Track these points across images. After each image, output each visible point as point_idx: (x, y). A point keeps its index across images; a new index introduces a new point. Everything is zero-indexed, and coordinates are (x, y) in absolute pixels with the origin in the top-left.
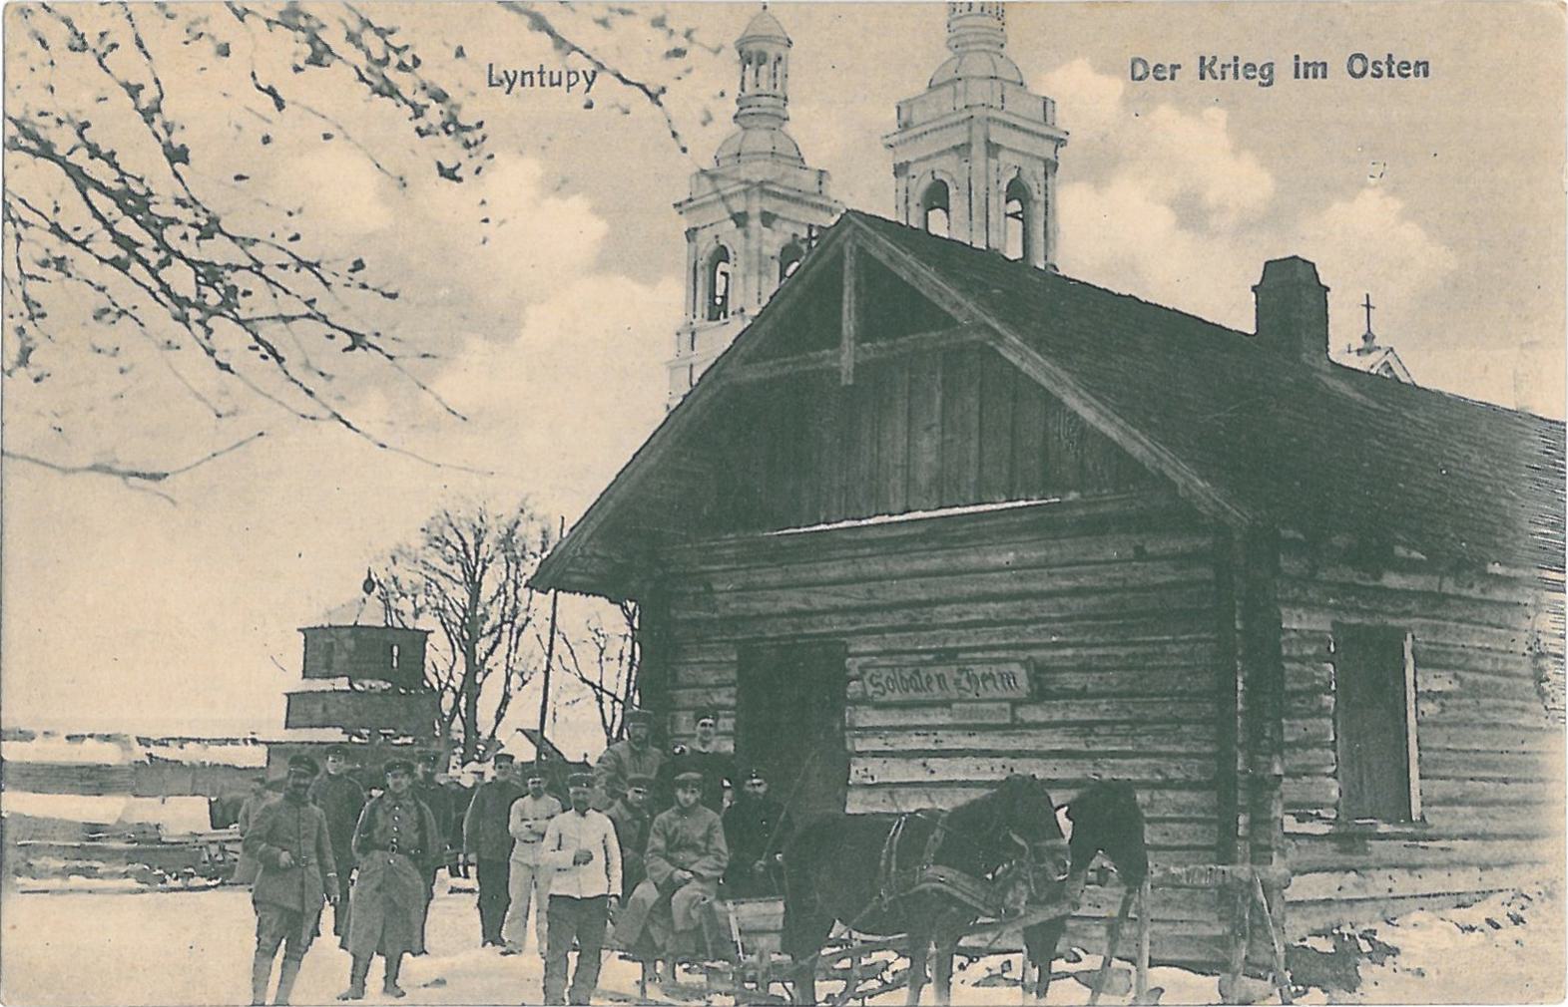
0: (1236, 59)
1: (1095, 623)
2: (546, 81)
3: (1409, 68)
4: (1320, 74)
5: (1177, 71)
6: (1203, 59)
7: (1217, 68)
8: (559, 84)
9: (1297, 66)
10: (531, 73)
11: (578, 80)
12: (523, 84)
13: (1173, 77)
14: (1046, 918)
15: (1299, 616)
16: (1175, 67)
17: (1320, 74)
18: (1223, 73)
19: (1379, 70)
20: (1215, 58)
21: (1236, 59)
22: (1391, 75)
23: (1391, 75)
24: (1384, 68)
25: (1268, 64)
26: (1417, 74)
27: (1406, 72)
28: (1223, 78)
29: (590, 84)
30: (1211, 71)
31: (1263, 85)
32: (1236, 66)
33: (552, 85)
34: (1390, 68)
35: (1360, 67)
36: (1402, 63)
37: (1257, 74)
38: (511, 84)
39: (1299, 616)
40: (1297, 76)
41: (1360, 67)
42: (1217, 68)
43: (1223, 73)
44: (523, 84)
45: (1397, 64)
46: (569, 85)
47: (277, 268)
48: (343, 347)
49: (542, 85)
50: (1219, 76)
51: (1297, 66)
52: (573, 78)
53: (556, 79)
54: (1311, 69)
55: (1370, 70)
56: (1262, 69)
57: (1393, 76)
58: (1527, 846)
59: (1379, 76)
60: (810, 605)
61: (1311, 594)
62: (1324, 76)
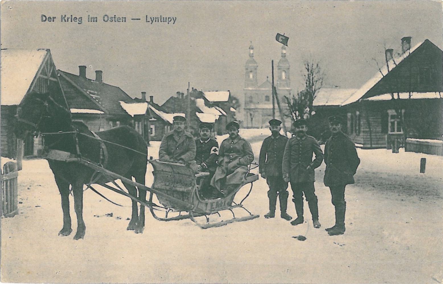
0: (72, 16)
2: (162, 20)
3: (77, 19)
5: (55, 19)
6: (62, 16)
7: (66, 18)
8: (91, 18)
12: (156, 21)
13: (53, 21)
15: (287, 158)
16: (54, 18)
17: (124, 21)
18: (68, 20)
19: (111, 19)
20: (65, 15)
21: (72, 16)
22: (161, 22)
27: (76, 20)
28: (68, 21)
29: (174, 22)
31: (79, 23)
34: (115, 19)
35: (106, 18)
36: (75, 18)
38: (152, 22)
39: (287, 158)
40: (89, 21)
41: (106, 18)
42: (66, 18)
43: (68, 20)
44: (156, 21)
46: (169, 21)
47: (106, 217)
48: (293, 236)
50: (66, 20)
51: (88, 18)
52: (170, 20)
55: (110, 19)
61: (421, 130)
62: (125, 21)
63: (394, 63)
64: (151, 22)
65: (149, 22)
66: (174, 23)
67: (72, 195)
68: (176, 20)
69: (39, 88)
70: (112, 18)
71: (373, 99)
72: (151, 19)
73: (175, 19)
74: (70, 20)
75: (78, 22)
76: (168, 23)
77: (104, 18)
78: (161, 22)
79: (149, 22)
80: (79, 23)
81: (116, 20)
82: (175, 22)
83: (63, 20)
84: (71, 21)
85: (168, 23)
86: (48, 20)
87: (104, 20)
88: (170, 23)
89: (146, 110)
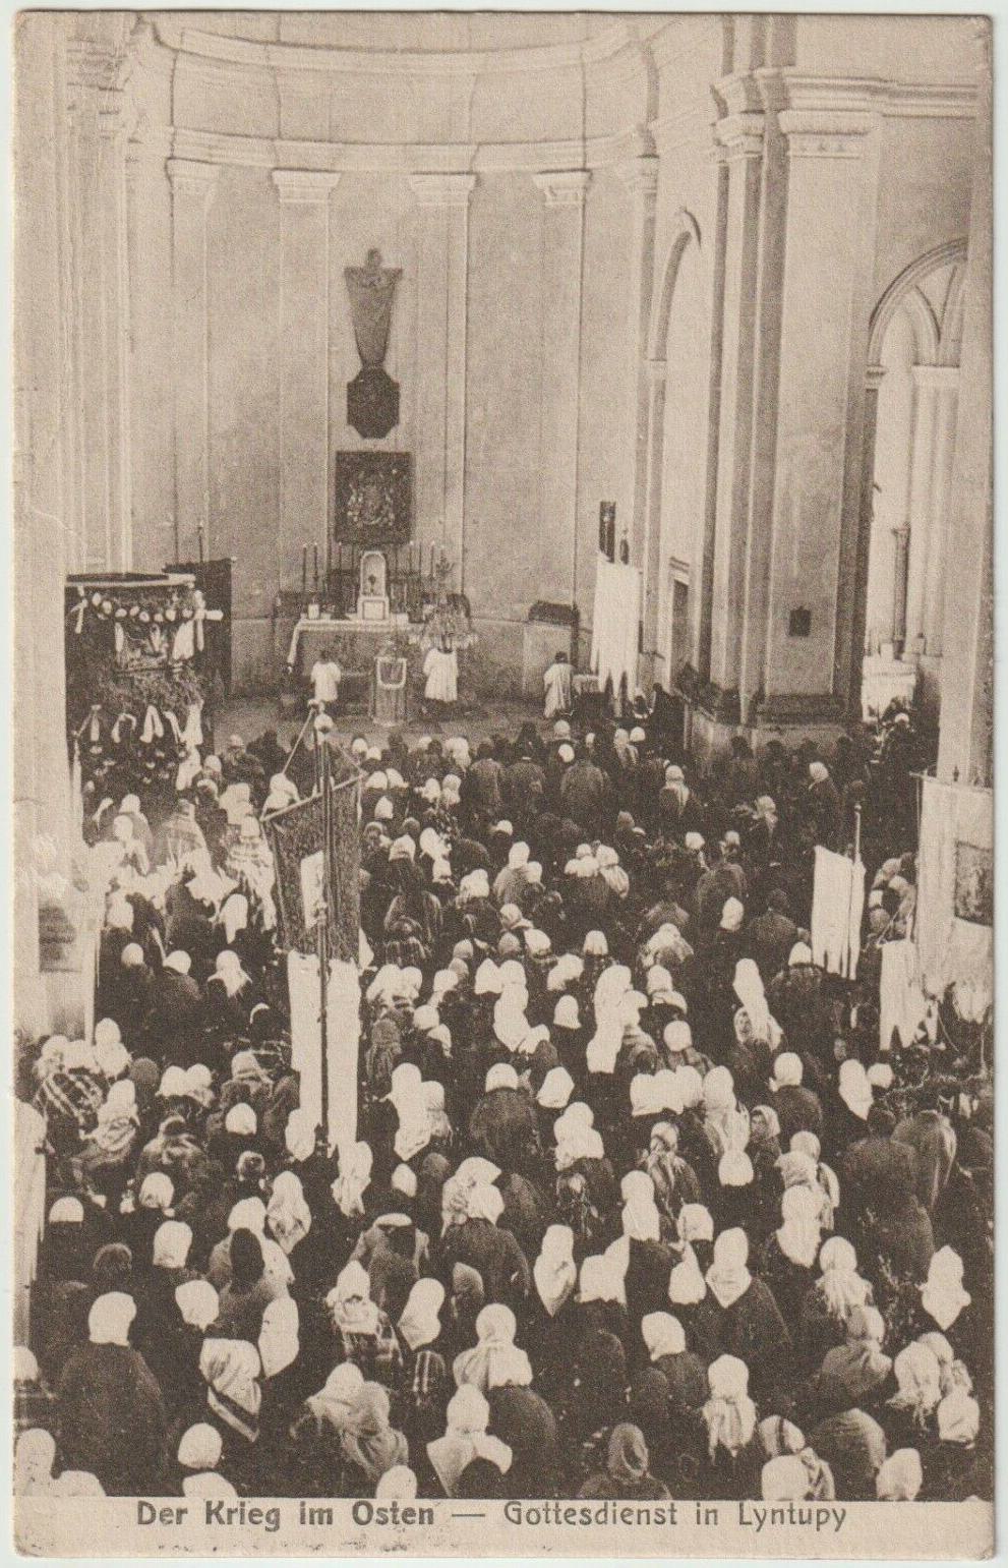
1: (647, 535)
2: (796, 1518)
4: (426, 1521)
5: (184, 1516)
6: (209, 1504)
9: (698, 1512)
10: (647, 1511)
11: (827, 1518)
13: (179, 1522)
14: (233, 600)
23: (312, 1522)
24: (389, 1515)
25: (273, 1510)
26: (421, 1522)
28: (230, 1523)
29: (840, 1523)
30: (217, 1515)
31: (267, 1529)
32: (242, 1511)
33: (802, 1522)
34: (394, 1517)
37: (263, 1519)
38: (761, 1522)
40: (698, 1523)
42: (223, 1513)
45: (563, 1512)
46: (819, 1523)
49: (793, 1522)
51: (698, 1512)
52: (823, 1516)
53: (805, 1518)
54: (316, 1516)
55: (375, 1516)
56: (268, 1513)
57: (560, 1523)
58: (776, 690)
59: (382, 1523)
60: (819, 1170)
63: (319, 1014)
64: (756, 1523)
65: (750, 1523)
66: (837, 1530)
67: (685, 1221)
68: (843, 1518)
69: (191, 140)
70: (386, 1510)
71: (736, 342)
72: (758, 1517)
73: (840, 1514)
74: (236, 1517)
75: (265, 1524)
76: (818, 1529)
77: (507, 1514)
78: (793, 1522)
79: (750, 1523)
80: (267, 1529)
81: (399, 1518)
82: (843, 1524)
83: (214, 1517)
84: (615, 1522)
85: (818, 1529)
86: (162, 1520)
87: (358, 1521)
88: (821, 1527)
89: (291, 1000)
